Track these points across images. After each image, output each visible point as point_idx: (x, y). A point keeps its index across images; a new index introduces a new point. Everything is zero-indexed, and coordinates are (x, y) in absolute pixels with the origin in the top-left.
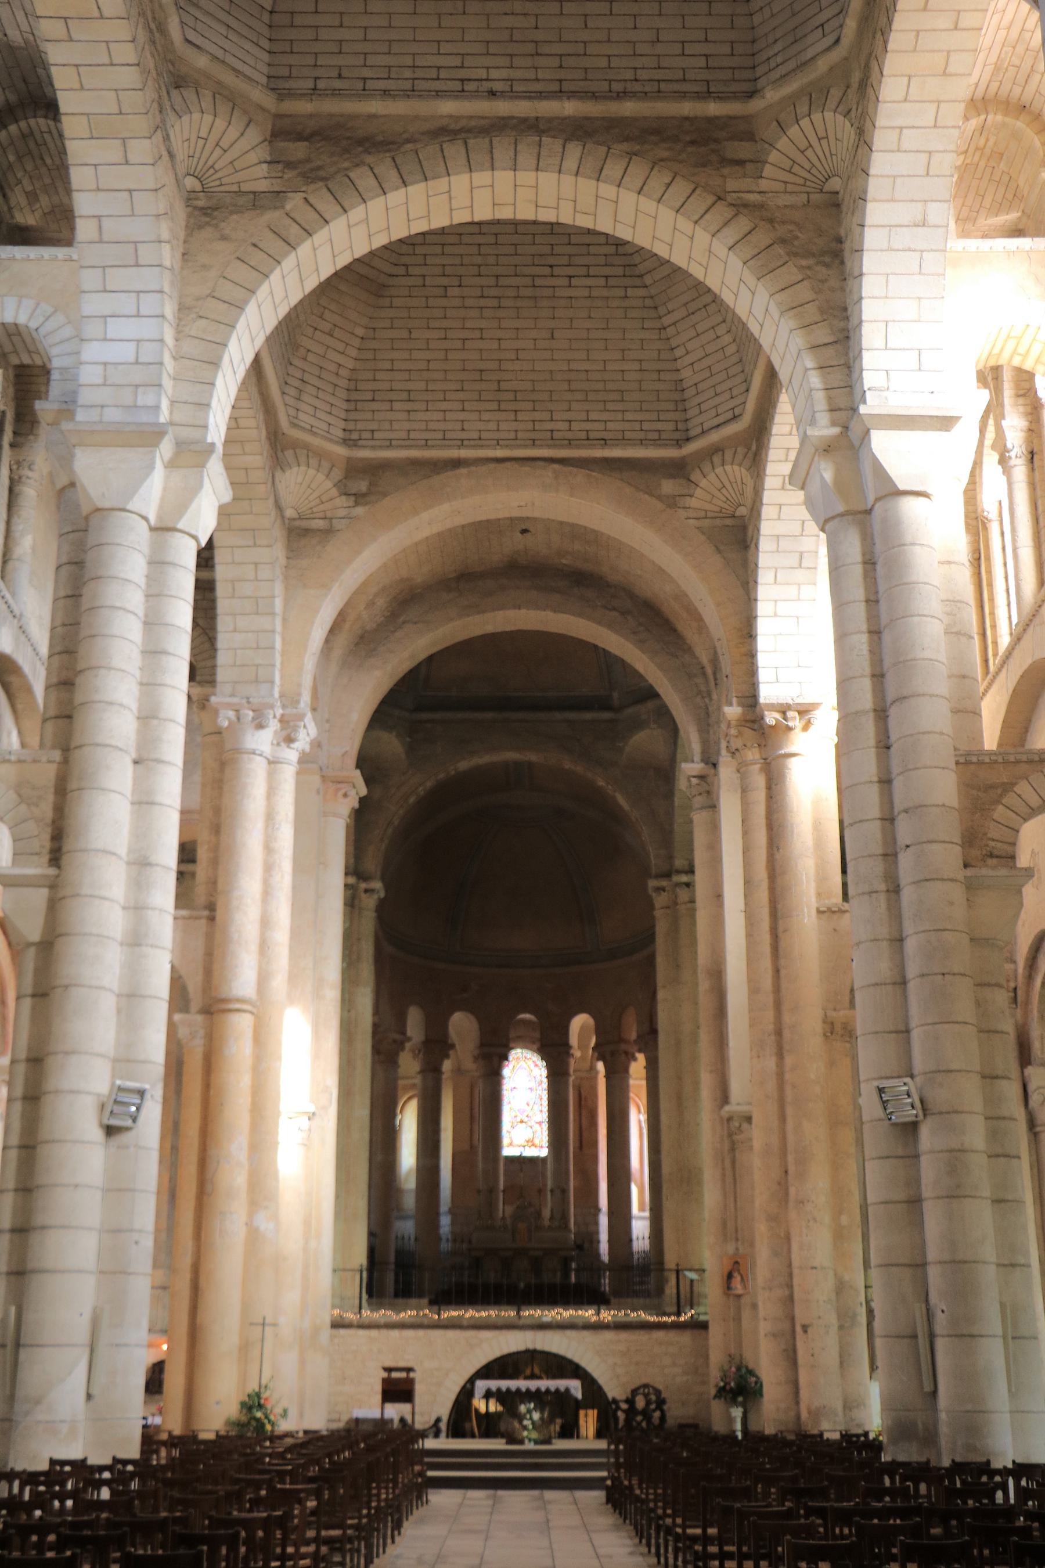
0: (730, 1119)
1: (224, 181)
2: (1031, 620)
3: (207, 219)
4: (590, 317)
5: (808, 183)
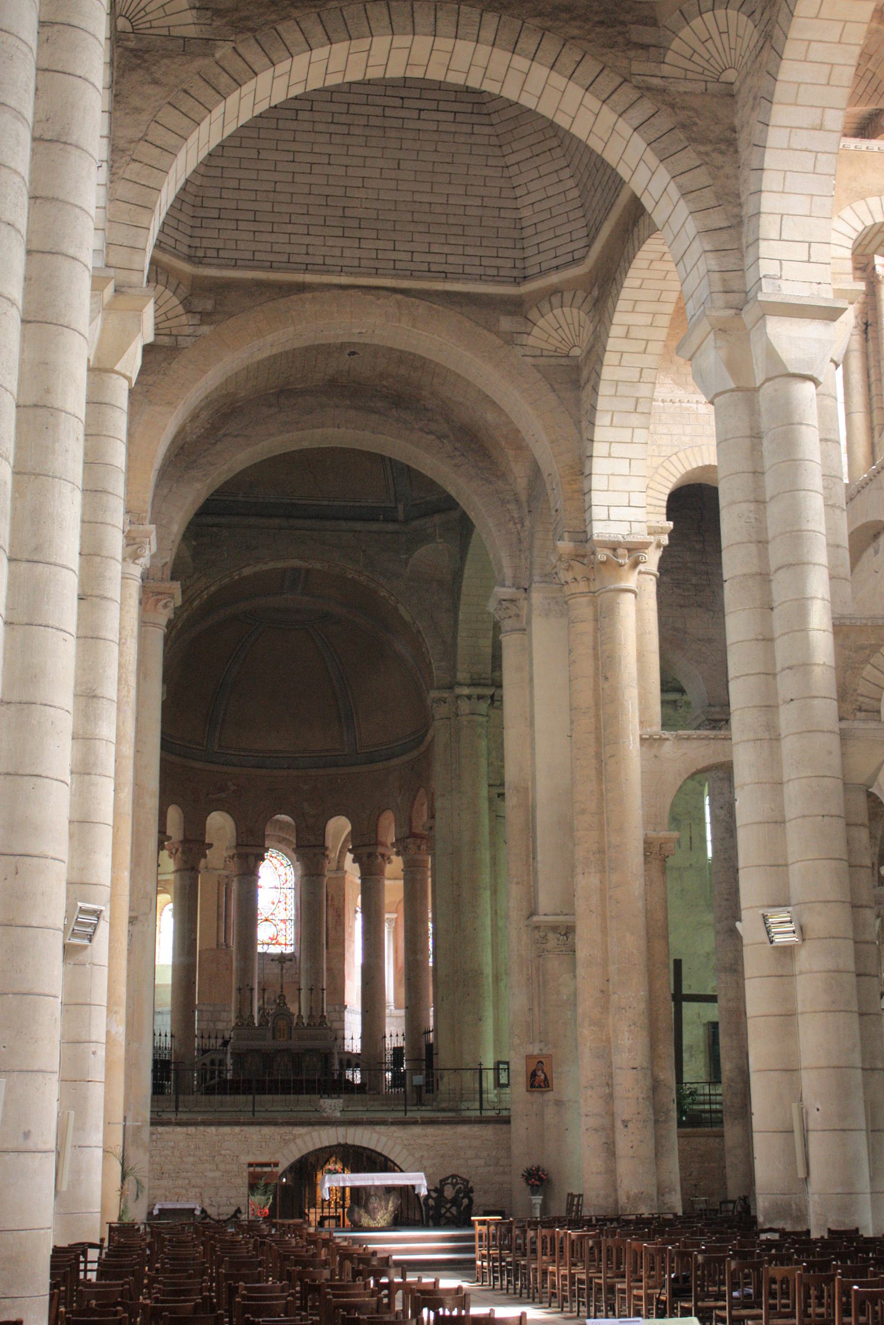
1: (155, 24)
2: (867, 484)
3: (139, 62)
4: (436, 151)
5: (706, 72)
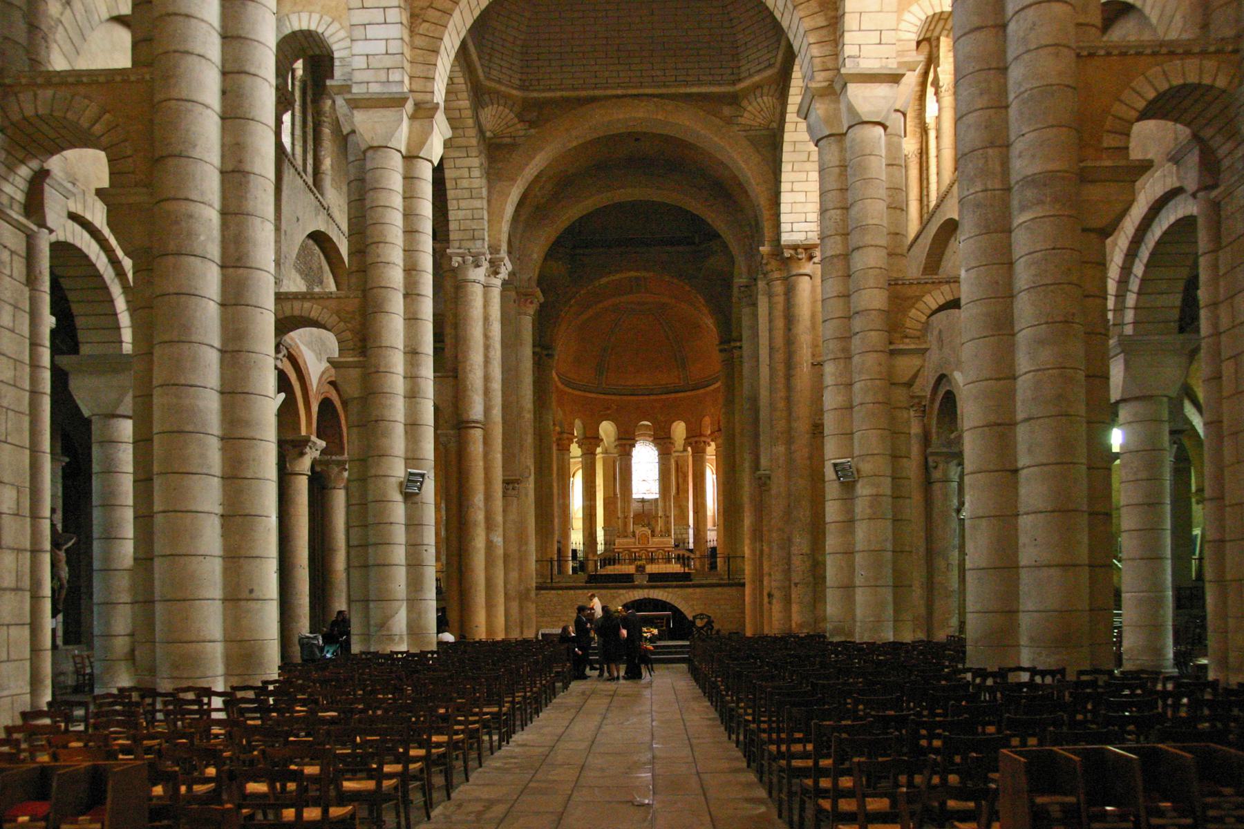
0: (760, 478)
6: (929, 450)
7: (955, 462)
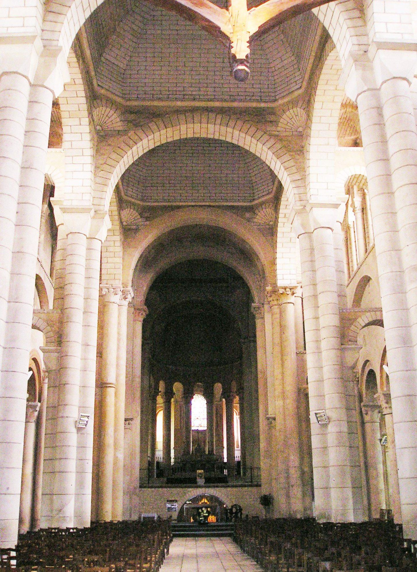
6: (362, 404)
7: (377, 411)
